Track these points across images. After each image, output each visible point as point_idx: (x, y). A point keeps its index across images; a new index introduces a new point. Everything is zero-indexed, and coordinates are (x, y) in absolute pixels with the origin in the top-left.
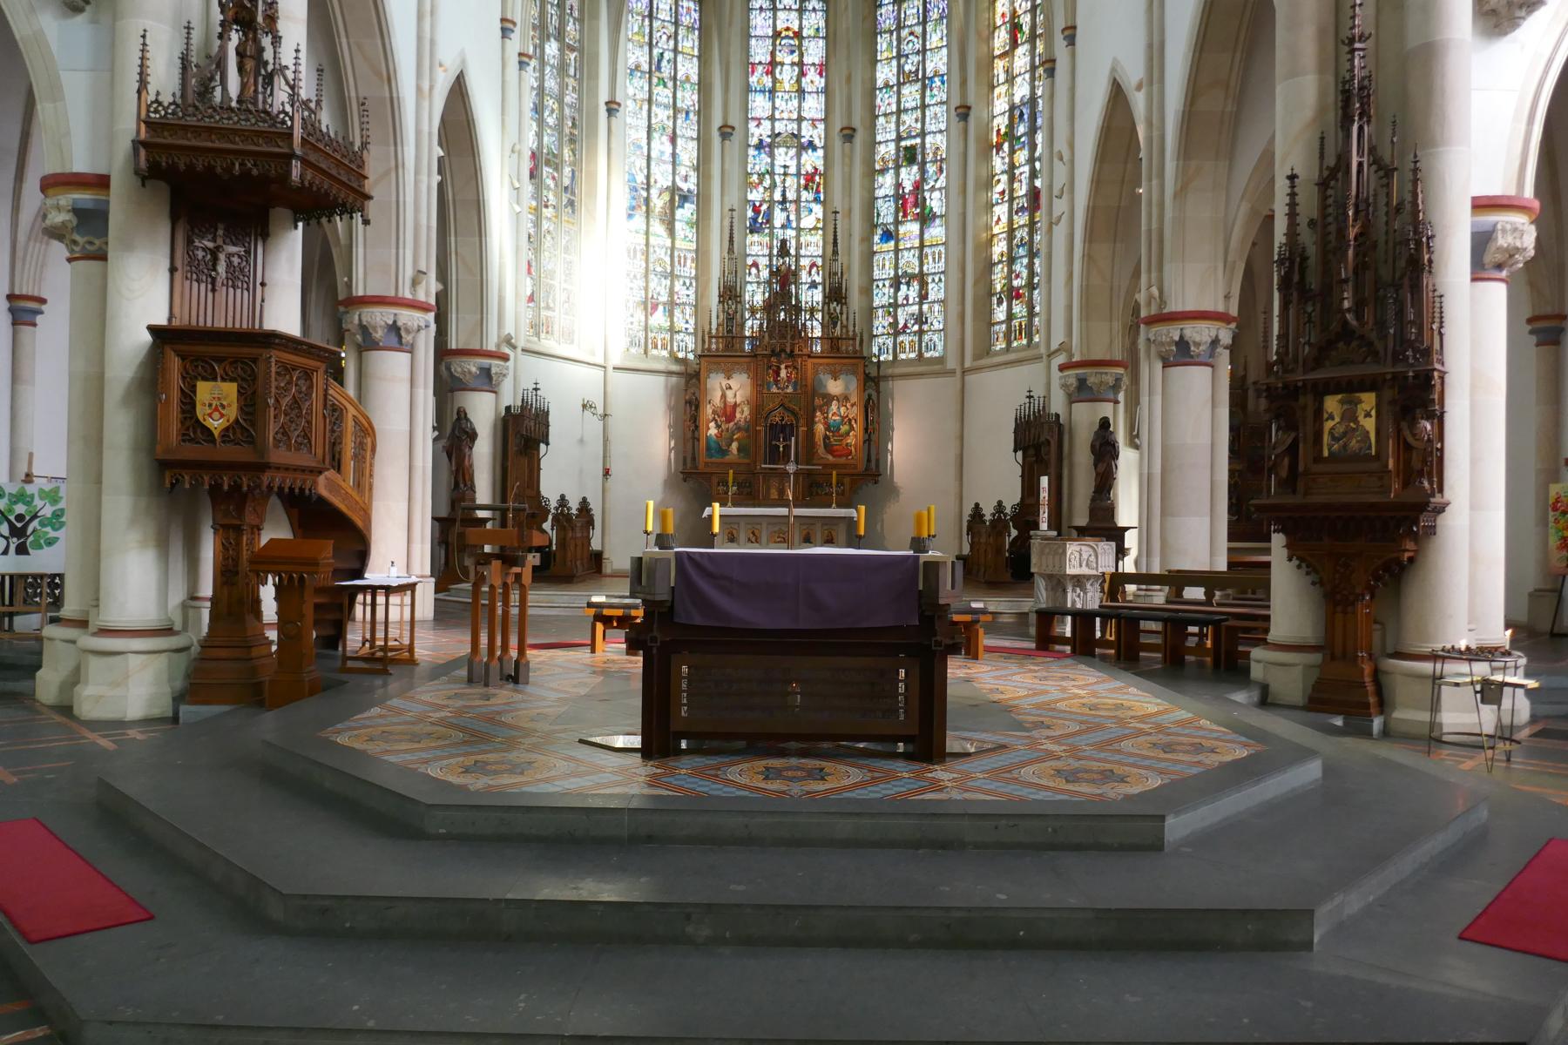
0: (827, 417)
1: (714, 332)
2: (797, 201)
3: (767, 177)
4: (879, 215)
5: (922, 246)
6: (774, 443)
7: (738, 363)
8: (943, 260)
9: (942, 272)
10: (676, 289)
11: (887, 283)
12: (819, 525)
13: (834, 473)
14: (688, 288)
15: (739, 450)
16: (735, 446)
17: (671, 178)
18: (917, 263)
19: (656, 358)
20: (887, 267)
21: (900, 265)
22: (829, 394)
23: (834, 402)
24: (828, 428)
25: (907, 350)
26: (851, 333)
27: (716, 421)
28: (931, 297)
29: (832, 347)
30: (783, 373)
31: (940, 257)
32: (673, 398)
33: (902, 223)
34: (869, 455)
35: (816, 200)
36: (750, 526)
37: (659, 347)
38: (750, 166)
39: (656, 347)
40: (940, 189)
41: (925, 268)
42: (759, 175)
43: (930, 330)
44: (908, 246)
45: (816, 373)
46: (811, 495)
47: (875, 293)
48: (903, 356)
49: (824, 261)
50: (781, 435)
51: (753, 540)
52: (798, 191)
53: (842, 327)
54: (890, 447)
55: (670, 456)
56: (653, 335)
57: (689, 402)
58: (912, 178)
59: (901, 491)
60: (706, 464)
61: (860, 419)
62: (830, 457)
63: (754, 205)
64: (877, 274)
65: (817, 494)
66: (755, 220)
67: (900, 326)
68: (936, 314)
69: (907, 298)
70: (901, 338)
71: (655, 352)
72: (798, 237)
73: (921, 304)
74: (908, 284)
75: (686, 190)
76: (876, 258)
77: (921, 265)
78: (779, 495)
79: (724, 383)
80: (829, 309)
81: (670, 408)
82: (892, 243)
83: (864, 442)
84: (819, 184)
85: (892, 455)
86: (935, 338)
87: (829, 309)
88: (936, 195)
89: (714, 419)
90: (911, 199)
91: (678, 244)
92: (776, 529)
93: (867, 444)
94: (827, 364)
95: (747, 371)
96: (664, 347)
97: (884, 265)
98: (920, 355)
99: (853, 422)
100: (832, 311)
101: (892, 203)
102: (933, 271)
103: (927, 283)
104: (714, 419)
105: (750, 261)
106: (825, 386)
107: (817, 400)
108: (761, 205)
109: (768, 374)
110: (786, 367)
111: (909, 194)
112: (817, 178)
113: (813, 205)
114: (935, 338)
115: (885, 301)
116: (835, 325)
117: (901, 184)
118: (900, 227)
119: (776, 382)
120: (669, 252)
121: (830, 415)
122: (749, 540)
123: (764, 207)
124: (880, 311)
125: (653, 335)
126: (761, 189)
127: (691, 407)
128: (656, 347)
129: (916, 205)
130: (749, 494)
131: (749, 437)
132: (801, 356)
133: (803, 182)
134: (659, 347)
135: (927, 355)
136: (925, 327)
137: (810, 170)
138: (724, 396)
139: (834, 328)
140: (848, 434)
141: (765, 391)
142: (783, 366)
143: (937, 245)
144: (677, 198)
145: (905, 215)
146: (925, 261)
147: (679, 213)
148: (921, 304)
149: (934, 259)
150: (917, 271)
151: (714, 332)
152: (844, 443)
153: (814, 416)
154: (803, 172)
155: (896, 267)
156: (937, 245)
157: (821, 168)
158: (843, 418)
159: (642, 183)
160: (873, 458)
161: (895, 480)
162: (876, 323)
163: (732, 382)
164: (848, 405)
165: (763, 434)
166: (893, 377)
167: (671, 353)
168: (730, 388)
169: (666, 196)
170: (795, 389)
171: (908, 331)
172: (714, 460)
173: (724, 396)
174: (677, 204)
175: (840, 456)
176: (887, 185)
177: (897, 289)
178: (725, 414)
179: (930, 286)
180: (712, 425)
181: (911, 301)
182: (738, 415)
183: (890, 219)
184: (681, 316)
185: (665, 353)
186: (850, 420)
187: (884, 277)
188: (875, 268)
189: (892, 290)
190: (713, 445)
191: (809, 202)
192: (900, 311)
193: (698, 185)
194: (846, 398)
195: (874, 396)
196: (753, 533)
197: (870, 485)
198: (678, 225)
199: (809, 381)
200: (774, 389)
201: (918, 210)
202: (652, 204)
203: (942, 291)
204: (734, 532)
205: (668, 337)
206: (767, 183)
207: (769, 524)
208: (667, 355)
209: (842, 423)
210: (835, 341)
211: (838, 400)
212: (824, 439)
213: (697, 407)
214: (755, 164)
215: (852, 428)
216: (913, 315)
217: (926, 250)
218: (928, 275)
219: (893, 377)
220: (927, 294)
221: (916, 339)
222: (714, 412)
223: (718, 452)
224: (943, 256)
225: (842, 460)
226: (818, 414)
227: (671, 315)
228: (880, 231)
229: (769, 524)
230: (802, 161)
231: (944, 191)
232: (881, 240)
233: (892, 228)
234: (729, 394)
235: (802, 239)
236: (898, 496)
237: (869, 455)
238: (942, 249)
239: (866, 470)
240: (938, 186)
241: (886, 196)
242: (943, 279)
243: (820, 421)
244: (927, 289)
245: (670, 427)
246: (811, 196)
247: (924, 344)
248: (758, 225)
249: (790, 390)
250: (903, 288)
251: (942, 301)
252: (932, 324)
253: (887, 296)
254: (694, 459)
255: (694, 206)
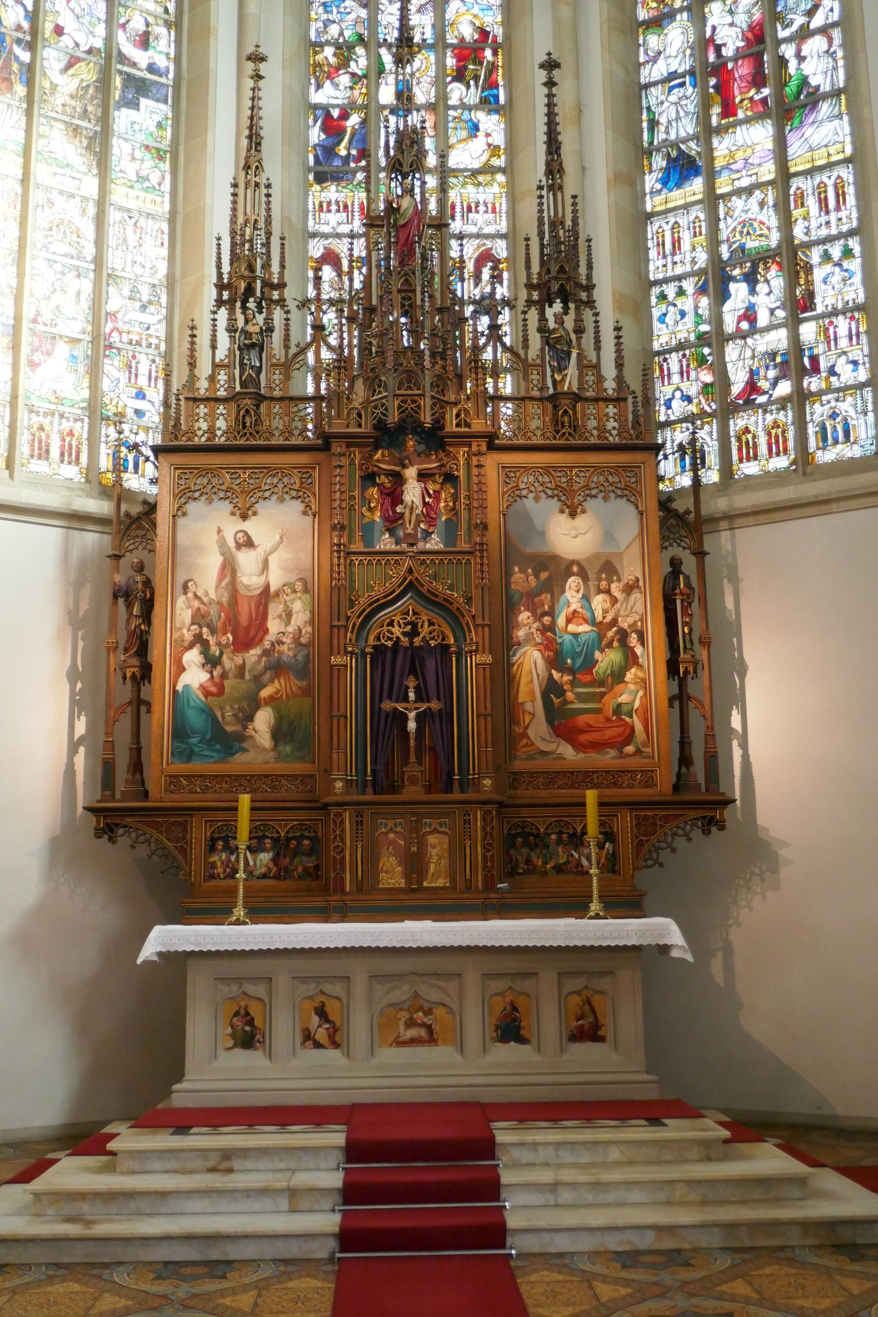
0: (552, 628)
1: (203, 385)
2: (439, 106)
3: (360, 51)
4: (653, 124)
5: (784, 175)
6: (387, 705)
7: (268, 469)
8: (851, 200)
9: (851, 233)
10: (111, 306)
11: (689, 286)
12: (548, 978)
13: (245, 800)
14: (144, 307)
15: (278, 734)
16: (263, 720)
17: (101, 30)
18: (773, 221)
19: (39, 481)
20: (686, 245)
21: (724, 234)
22: (554, 558)
23: (573, 582)
24: (555, 660)
25: (763, 449)
26: (610, 385)
27: (205, 644)
28: (825, 299)
29: (556, 422)
30: (413, 492)
31: (840, 196)
32: (86, 592)
33: (721, 131)
34: (684, 743)
35: (488, 103)
36: (310, 989)
37: (55, 453)
38: (314, 27)
39: (44, 454)
40: (824, 30)
41: (798, 232)
42: (338, 47)
43: (829, 390)
44: (745, 182)
45: (515, 495)
46: (511, 873)
47: (656, 313)
48: (751, 468)
49: (512, 248)
50: (411, 683)
51: (321, 1035)
52: (440, 83)
53: (582, 366)
54: (736, 721)
55: (70, 764)
56: (36, 420)
57: (123, 594)
58: (742, 20)
59: (783, 852)
60: (173, 779)
61: (655, 631)
62: (567, 751)
63: (328, 116)
64: (656, 268)
65: (531, 870)
66: (328, 151)
67: (736, 389)
68: (843, 343)
69: (750, 315)
70: (737, 424)
71: (38, 466)
72: (443, 188)
73: (794, 323)
74: (751, 279)
75: (144, 65)
76: (651, 229)
77: (787, 223)
78: (407, 875)
79: (232, 527)
80: (543, 318)
81: (74, 620)
82: (697, 184)
83: (671, 700)
84: (492, 68)
85: (744, 745)
86: (846, 407)
87: (543, 318)
88: (817, 44)
89: (199, 639)
90: (743, 70)
91: (118, 194)
92: (401, 993)
93: (677, 704)
94: (547, 470)
95: (300, 493)
96: (69, 455)
97: (676, 244)
98: (804, 458)
99: (633, 640)
100: (552, 324)
101: (690, 90)
102: (824, 232)
103: (809, 269)
104: (199, 639)
105: (316, 249)
106: (542, 534)
107: (518, 577)
108: (345, 116)
109: (365, 501)
110: (422, 476)
111: (735, 60)
112: (488, 54)
113: (480, 116)
114: (846, 407)
115: (686, 330)
116: (562, 358)
117: (712, 39)
118: (715, 142)
119: (393, 522)
120: (92, 210)
121: (561, 621)
122: (308, 1037)
123: (354, 120)
124: (674, 360)
125: (36, 420)
126: (344, 80)
127: (129, 606)
128: (44, 454)
129: (758, 80)
130: (313, 873)
131: (307, 692)
132: (466, 439)
133: (451, 62)
134: (55, 453)
135: (827, 456)
136: (813, 383)
137: (468, 33)
138: (229, 568)
139: (561, 369)
140: (618, 676)
141: (355, 547)
142: (411, 473)
143: (830, 166)
144: (118, 81)
145: (729, 110)
146: (797, 213)
147: (122, 118)
148: (794, 323)
149: (823, 203)
150: (775, 238)
151: (203, 385)
152: (610, 704)
153: (509, 623)
154: (451, 39)
155: (714, 242)
156: (830, 166)
157: (498, 31)
158: (601, 627)
159: (19, 28)
160: (698, 753)
161: (760, 821)
162: (662, 391)
163: (251, 526)
164: (616, 589)
165: (351, 677)
166: (731, 518)
167: (91, 473)
168: (249, 544)
169: (87, 73)
170: (450, 535)
171: (762, 399)
172: (197, 766)
173: (229, 568)
174: (117, 95)
175: (597, 746)
176: (672, 51)
177: (723, 296)
178: (231, 622)
179: (818, 274)
180: (192, 657)
181: (763, 320)
182: (274, 626)
183: (688, 127)
184: (123, 377)
185: (71, 472)
186: (623, 636)
187: (679, 270)
188: (653, 254)
189: (704, 301)
190: (195, 719)
191: (469, 108)
192: (732, 351)
193: (177, 60)
194: (609, 569)
195: (689, 564)
196: (322, 1013)
197: (680, 842)
198: (119, 148)
199: (493, 518)
200: (385, 542)
201: (766, 91)
202: (44, 83)
203: (857, 279)
204: (255, 1010)
205: (82, 429)
206: (360, 63)
207: (375, 977)
208: (79, 479)
209: (601, 643)
210: (565, 402)
211: (583, 575)
212: (545, 695)
213: (148, 605)
214: (327, 23)
215: (631, 659)
216: (773, 355)
217: (796, 184)
218: (809, 245)
219: (731, 518)
220: (810, 295)
221: (787, 417)
222: (199, 618)
223: (209, 743)
224: (850, 190)
225: (608, 759)
226: (524, 616)
227: (95, 372)
228: (659, 162)
229: (375, 977)
230: (450, 15)
231: (836, 34)
232: (665, 182)
233: (693, 148)
234: (247, 561)
235: (453, 195)
236: (775, 870)
237: (684, 743)
238: (846, 174)
239: (676, 788)
240: (818, 21)
241: (672, 76)
242: (857, 250)
243: (529, 638)
244: (809, 283)
245: (73, 675)
246: (473, 96)
247: (811, 430)
248: (337, 163)
249: (435, 543)
250: (739, 290)
251: (858, 308)
252: (832, 372)
253: (690, 319)
254: (137, 766)
255: (165, 109)
